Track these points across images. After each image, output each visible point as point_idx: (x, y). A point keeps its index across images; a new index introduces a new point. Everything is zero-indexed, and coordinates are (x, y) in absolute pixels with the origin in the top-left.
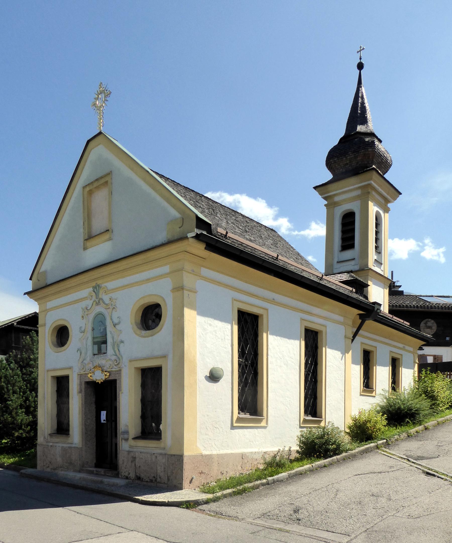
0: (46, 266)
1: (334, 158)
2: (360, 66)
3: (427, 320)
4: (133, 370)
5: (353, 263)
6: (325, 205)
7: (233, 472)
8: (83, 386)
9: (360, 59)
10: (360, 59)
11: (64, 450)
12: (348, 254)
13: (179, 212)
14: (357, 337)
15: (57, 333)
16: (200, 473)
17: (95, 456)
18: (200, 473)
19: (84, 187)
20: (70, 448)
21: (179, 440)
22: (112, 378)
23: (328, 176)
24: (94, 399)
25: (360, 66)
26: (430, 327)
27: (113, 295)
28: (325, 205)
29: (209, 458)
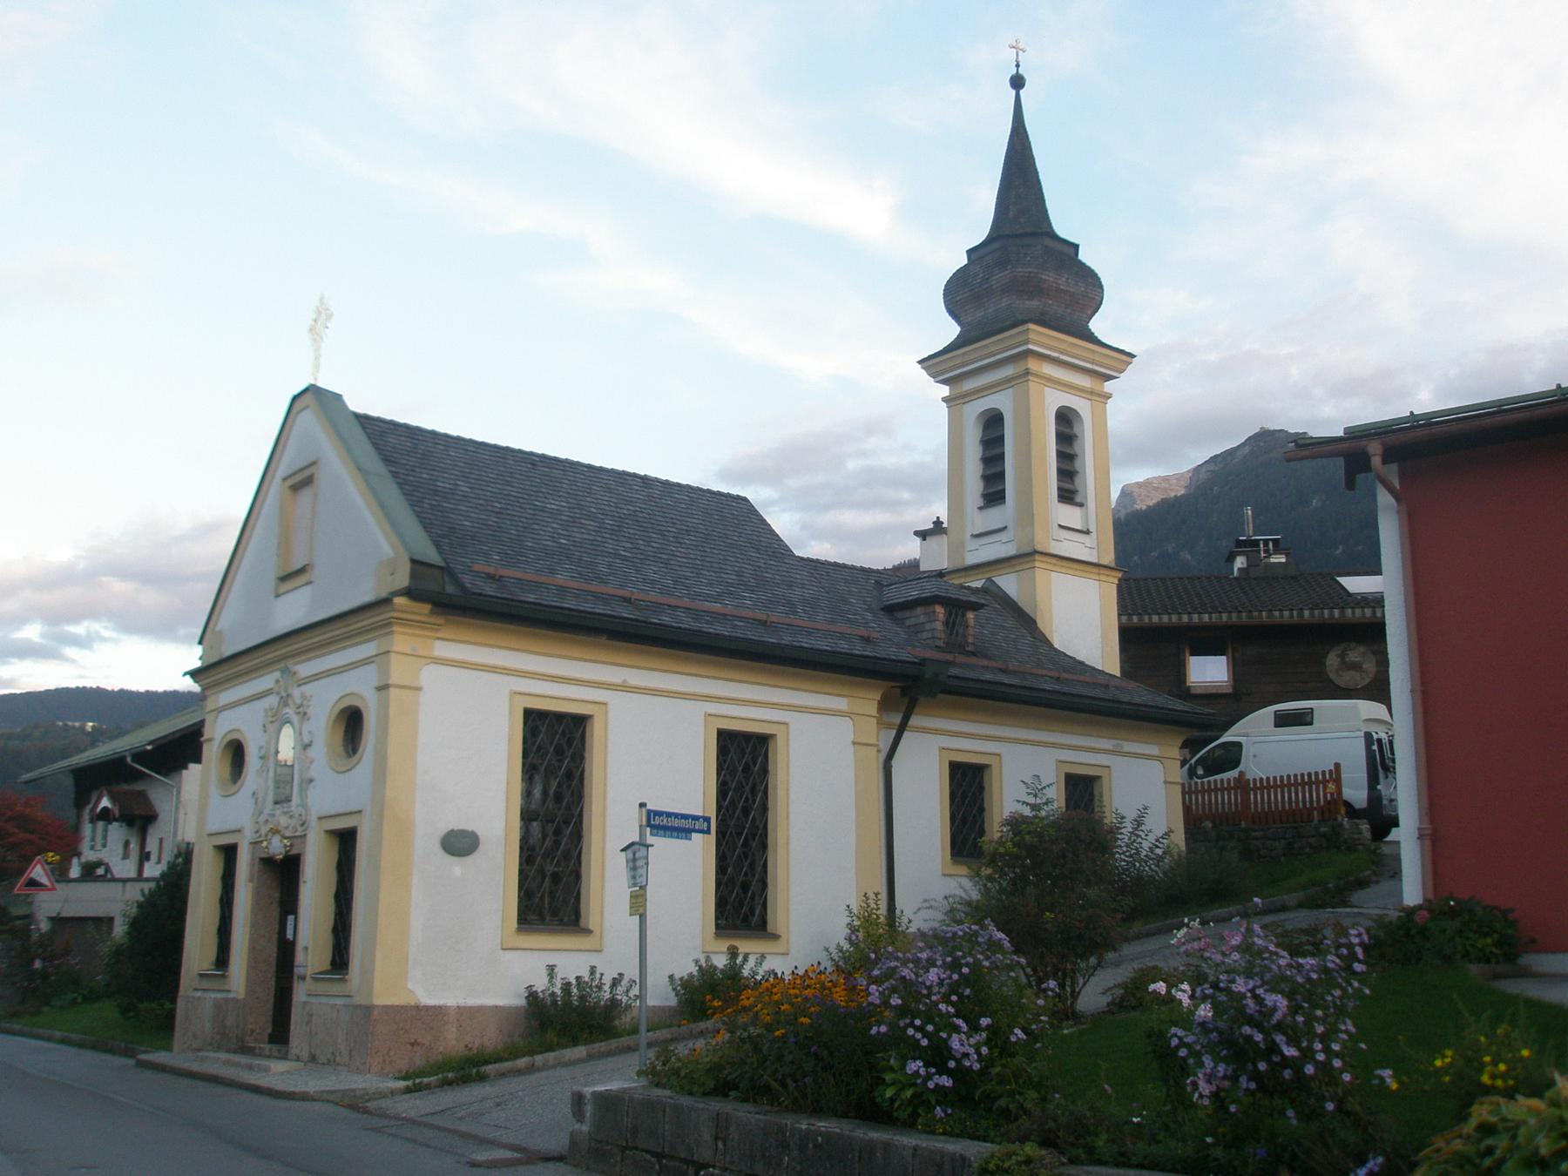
0: (225, 621)
1: (962, 293)
2: (1017, 82)
3: (1344, 645)
4: (323, 835)
5: (1002, 537)
6: (945, 400)
7: (452, 1042)
8: (256, 868)
9: (1018, 66)
10: (1018, 66)
11: (218, 1006)
12: (995, 517)
13: (427, 526)
14: (906, 735)
15: (346, 732)
16: (412, 1045)
17: (270, 1019)
18: (412, 1045)
19: (285, 479)
20: (226, 1000)
21: (368, 973)
22: (294, 852)
23: (952, 330)
24: (277, 895)
25: (1017, 82)
26: (1356, 667)
27: (307, 689)
28: (945, 400)
29: (438, 1012)
